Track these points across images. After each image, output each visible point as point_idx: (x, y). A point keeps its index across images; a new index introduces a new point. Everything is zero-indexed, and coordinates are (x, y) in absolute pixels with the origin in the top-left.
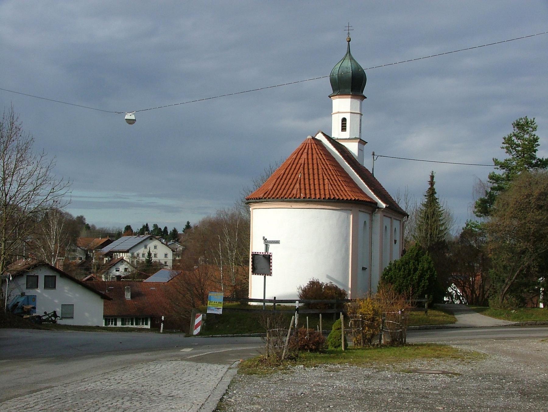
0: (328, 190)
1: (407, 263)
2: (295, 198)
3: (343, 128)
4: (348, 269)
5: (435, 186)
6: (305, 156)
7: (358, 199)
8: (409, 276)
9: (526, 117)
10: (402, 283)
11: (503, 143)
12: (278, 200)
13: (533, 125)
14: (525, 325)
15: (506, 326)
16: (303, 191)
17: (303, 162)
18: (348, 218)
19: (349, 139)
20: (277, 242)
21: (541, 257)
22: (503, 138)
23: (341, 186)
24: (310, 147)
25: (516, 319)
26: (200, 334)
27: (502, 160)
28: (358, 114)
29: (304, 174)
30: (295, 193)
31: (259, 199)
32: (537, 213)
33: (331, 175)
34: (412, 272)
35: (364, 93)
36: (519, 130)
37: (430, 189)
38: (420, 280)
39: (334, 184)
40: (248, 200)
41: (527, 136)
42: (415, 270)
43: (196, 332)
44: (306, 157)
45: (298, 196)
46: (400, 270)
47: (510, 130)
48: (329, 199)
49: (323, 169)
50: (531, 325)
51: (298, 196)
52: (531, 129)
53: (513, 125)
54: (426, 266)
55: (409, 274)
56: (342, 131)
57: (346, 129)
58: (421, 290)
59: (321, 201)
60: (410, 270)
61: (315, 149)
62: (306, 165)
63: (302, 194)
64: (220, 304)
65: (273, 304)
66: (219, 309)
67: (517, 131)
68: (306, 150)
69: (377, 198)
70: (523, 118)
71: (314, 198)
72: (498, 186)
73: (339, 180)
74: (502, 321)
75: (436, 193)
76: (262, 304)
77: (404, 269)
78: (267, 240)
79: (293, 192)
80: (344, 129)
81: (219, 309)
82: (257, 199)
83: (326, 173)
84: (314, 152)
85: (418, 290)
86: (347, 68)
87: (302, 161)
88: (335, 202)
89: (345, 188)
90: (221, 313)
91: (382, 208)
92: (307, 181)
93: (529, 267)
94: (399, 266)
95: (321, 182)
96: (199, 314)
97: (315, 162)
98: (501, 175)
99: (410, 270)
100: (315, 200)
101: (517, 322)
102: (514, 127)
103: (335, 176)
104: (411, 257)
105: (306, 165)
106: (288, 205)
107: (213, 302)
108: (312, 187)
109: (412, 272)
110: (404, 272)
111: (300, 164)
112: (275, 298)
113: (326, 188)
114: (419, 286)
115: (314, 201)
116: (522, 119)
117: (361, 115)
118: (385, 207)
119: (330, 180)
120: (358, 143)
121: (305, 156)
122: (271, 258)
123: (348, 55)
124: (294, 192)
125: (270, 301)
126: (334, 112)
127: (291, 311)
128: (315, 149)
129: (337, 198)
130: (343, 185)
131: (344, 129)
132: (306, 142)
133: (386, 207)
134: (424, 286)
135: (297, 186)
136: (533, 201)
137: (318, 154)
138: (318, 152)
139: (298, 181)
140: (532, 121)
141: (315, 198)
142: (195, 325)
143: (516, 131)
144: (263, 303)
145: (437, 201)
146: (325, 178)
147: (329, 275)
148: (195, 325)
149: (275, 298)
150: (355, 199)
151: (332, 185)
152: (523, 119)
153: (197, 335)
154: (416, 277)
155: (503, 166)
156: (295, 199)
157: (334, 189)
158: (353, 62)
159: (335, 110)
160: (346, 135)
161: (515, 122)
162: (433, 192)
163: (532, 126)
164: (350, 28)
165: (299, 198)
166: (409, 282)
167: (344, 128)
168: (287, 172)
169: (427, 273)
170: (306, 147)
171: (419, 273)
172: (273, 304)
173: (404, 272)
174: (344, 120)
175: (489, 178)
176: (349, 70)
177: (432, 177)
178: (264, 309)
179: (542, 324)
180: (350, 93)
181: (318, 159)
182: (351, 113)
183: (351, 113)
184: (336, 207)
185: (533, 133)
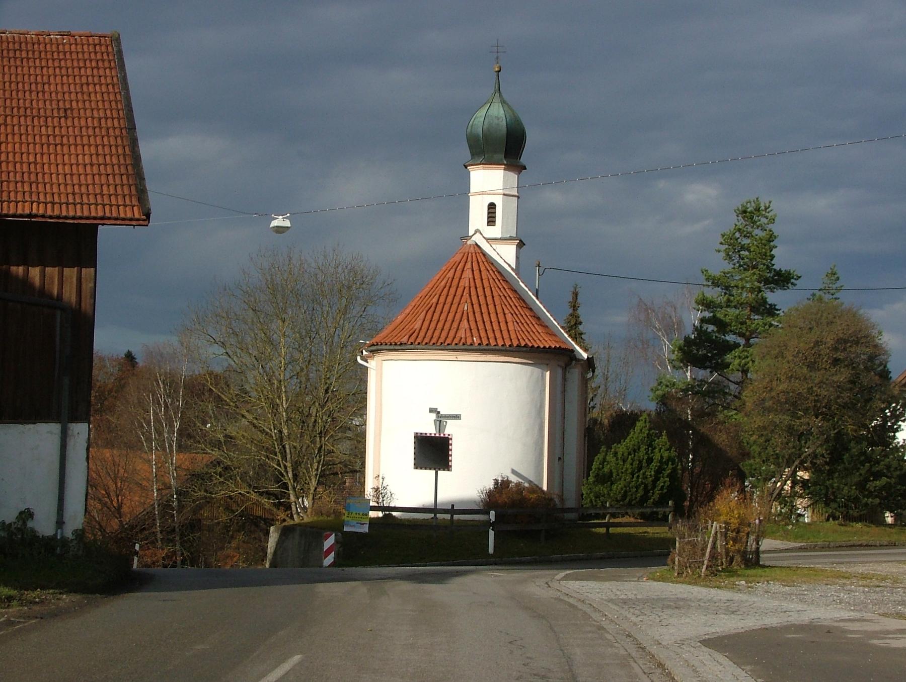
0: (516, 333)
2: (464, 344)
3: (490, 219)
4: (542, 460)
5: (580, 311)
6: (468, 274)
7: (560, 347)
8: (639, 471)
9: (757, 199)
11: (721, 243)
12: (434, 348)
13: (768, 213)
14: (814, 548)
15: (787, 549)
16: (475, 331)
17: (467, 285)
18: (543, 377)
19: (501, 239)
20: (457, 417)
22: (722, 235)
23: (530, 325)
24: (474, 259)
25: (800, 540)
26: (333, 565)
27: (716, 272)
30: (463, 336)
31: (401, 344)
33: (513, 307)
34: (644, 464)
35: (523, 160)
36: (745, 220)
37: (571, 315)
38: (657, 479)
39: (521, 322)
40: (377, 344)
41: (757, 232)
42: (650, 461)
43: (329, 560)
44: (471, 276)
45: (469, 341)
46: (624, 461)
47: (732, 221)
48: (518, 346)
49: (500, 296)
50: (823, 548)
51: (469, 341)
52: (765, 221)
53: (735, 211)
54: (666, 454)
55: (640, 469)
56: (488, 225)
57: (495, 222)
58: (658, 494)
59: (506, 351)
60: (640, 462)
61: (483, 262)
62: (473, 289)
63: (475, 339)
64: (365, 517)
65: (433, 515)
66: (363, 524)
67: (741, 222)
68: (469, 265)
69: (573, 343)
70: (752, 200)
71: (495, 345)
73: (526, 315)
74: (778, 542)
75: (581, 323)
76: (448, 517)
77: (632, 459)
78: (441, 413)
79: (458, 335)
80: (492, 222)
81: (363, 524)
82: (396, 344)
83: (506, 303)
84: (482, 268)
85: (653, 493)
86: (498, 119)
87: (465, 282)
88: (526, 352)
89: (538, 329)
90: (368, 531)
91: (582, 360)
92: (478, 315)
94: (623, 455)
95: (501, 319)
96: (328, 533)
97: (486, 284)
98: (715, 297)
99: (640, 462)
100: (488, 347)
101: (803, 544)
102: (738, 216)
103: (519, 307)
104: (642, 439)
105: (473, 289)
106: (452, 355)
107: (354, 513)
109: (644, 464)
110: (632, 464)
111: (463, 288)
112: (453, 506)
113: (511, 328)
114: (654, 486)
115: (495, 350)
116: (750, 202)
117: (518, 197)
118: (586, 357)
119: (514, 315)
120: (515, 246)
121: (468, 274)
122: (450, 442)
123: (497, 94)
124: (461, 333)
125: (445, 511)
126: (472, 190)
127: (481, 529)
128: (483, 262)
129: (530, 345)
130: (534, 323)
131: (492, 222)
132: (467, 251)
133: (588, 357)
134: (662, 487)
135: (465, 324)
137: (488, 271)
138: (489, 269)
140: (767, 205)
142: (333, 553)
143: (740, 223)
144: (450, 515)
145: (583, 336)
146: (506, 311)
147: (515, 469)
148: (333, 553)
149: (453, 506)
150: (555, 347)
151: (518, 323)
152: (752, 203)
153: (329, 566)
154: (650, 472)
155: (716, 282)
157: (522, 330)
158: (506, 107)
159: (474, 188)
160: (495, 231)
161: (740, 208)
162: (576, 320)
163: (767, 214)
164: (500, 49)
165: (471, 345)
166: (640, 480)
167: (491, 221)
168: (442, 300)
169: (668, 466)
170: (467, 258)
171: (656, 466)
172: (433, 515)
173: (632, 464)
174: (492, 207)
175: (696, 302)
176: (502, 121)
177: (576, 295)
178: (59, 538)
179: (837, 547)
180: (502, 160)
181: (491, 280)
182: (504, 195)
183: (504, 195)
184: (528, 359)
185: (770, 226)
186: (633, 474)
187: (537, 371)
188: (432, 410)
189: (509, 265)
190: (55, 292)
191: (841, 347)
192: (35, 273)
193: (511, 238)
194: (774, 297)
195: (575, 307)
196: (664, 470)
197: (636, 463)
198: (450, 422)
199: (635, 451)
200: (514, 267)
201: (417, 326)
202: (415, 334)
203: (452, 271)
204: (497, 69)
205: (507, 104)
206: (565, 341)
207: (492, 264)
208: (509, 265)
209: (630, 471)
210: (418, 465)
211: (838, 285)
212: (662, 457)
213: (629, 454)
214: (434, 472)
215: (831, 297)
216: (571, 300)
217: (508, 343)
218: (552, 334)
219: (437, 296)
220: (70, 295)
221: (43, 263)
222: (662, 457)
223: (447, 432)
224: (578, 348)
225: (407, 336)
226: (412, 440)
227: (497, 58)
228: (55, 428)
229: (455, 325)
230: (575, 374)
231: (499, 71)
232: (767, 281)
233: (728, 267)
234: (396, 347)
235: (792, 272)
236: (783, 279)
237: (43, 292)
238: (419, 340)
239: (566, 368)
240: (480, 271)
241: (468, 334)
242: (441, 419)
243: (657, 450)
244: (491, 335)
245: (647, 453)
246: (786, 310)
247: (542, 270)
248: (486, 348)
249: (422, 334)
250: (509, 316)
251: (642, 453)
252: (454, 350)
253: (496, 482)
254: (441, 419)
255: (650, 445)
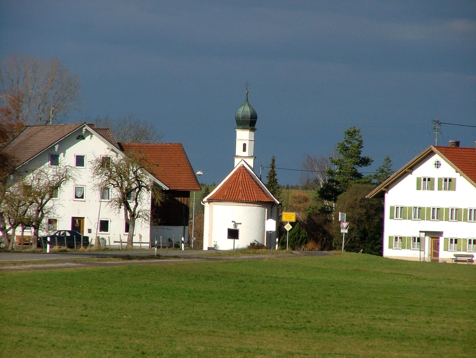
0: (257, 196)
1: (294, 235)
4: (264, 237)
6: (241, 177)
10: (292, 245)
16: (244, 196)
18: (265, 210)
20: (240, 224)
21: (361, 232)
27: (336, 159)
28: (253, 141)
29: (243, 187)
30: (240, 198)
31: (220, 200)
32: (360, 209)
35: (256, 126)
37: (271, 171)
42: (299, 238)
44: (242, 178)
48: (258, 201)
53: (345, 132)
54: (304, 236)
55: (296, 240)
56: (243, 151)
60: (296, 238)
62: (243, 182)
67: (348, 137)
68: (241, 173)
72: (347, 221)
75: (276, 175)
82: (218, 200)
84: (245, 175)
86: (247, 112)
87: (240, 180)
93: (355, 237)
102: (345, 135)
105: (243, 182)
106: (237, 204)
108: (248, 195)
113: (255, 195)
115: (252, 203)
121: (241, 177)
123: (247, 102)
124: (240, 197)
136: (358, 203)
139: (240, 191)
141: (251, 201)
145: (277, 181)
146: (253, 190)
147: (255, 240)
156: (241, 201)
160: (246, 154)
165: (243, 201)
167: (244, 150)
174: (245, 145)
177: (274, 161)
182: (249, 140)
183: (249, 140)
186: (293, 242)
187: (263, 209)
188: (233, 222)
189: (249, 166)
190: (183, 202)
191: (363, 201)
192: (179, 198)
193: (252, 157)
194: (361, 170)
195: (273, 167)
196: (303, 241)
197: (294, 239)
198: (238, 225)
199: (294, 235)
200: (252, 166)
201: (225, 194)
202: (225, 197)
203: (236, 176)
204: (247, 93)
205: (251, 106)
206: (272, 199)
207: (249, 173)
208: (249, 166)
209: (292, 241)
210: (228, 238)
211: (391, 163)
212: (303, 237)
213: (292, 236)
214: (233, 240)
215: (387, 169)
216: (272, 163)
217: (254, 200)
218: (268, 196)
219: (231, 184)
220: (185, 203)
221: (181, 197)
222: (303, 237)
223: (238, 228)
224: (276, 200)
225: (222, 198)
226: (227, 230)
227: (247, 88)
228: (183, 227)
229: (237, 194)
230: (275, 208)
231: (247, 93)
232: (357, 164)
233: (342, 157)
234: (219, 201)
235: (370, 158)
236: (365, 162)
237: (181, 202)
238: (228, 199)
239: (273, 206)
240: (245, 176)
241: (242, 197)
242: (236, 224)
243: (301, 235)
244: (249, 198)
245: (298, 235)
246: (366, 177)
247: (262, 167)
248: (247, 202)
249: (227, 197)
250: (254, 191)
251: (296, 236)
252: (237, 202)
253: (251, 244)
254: (236, 224)
255: (299, 233)
